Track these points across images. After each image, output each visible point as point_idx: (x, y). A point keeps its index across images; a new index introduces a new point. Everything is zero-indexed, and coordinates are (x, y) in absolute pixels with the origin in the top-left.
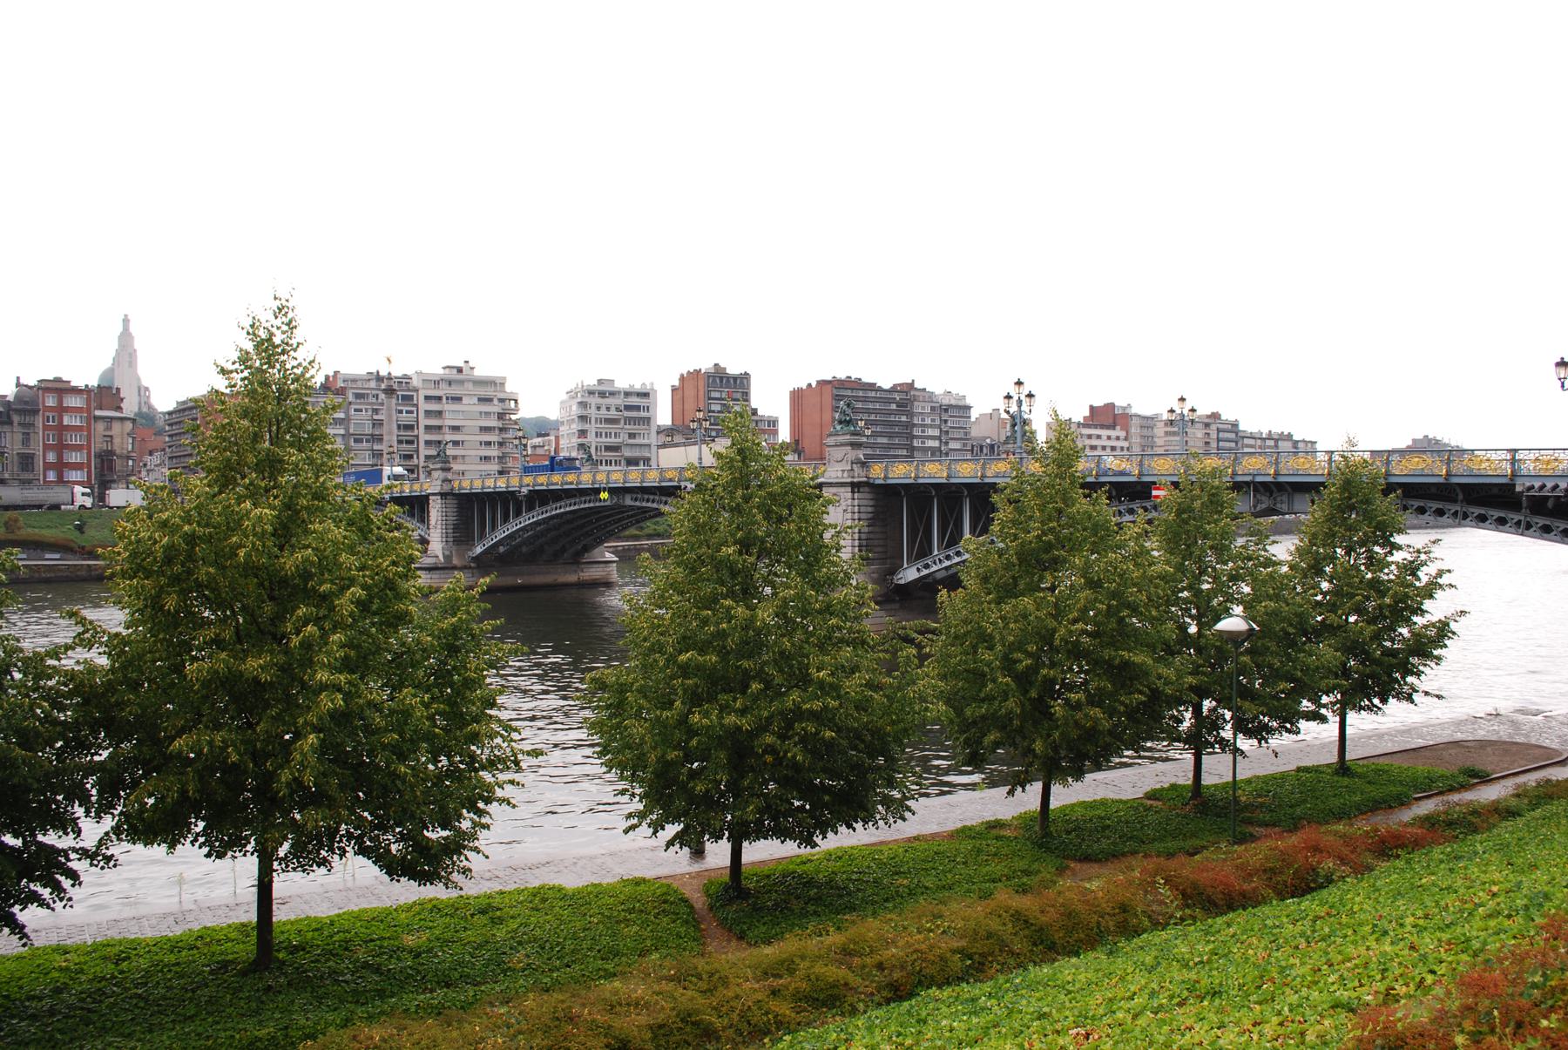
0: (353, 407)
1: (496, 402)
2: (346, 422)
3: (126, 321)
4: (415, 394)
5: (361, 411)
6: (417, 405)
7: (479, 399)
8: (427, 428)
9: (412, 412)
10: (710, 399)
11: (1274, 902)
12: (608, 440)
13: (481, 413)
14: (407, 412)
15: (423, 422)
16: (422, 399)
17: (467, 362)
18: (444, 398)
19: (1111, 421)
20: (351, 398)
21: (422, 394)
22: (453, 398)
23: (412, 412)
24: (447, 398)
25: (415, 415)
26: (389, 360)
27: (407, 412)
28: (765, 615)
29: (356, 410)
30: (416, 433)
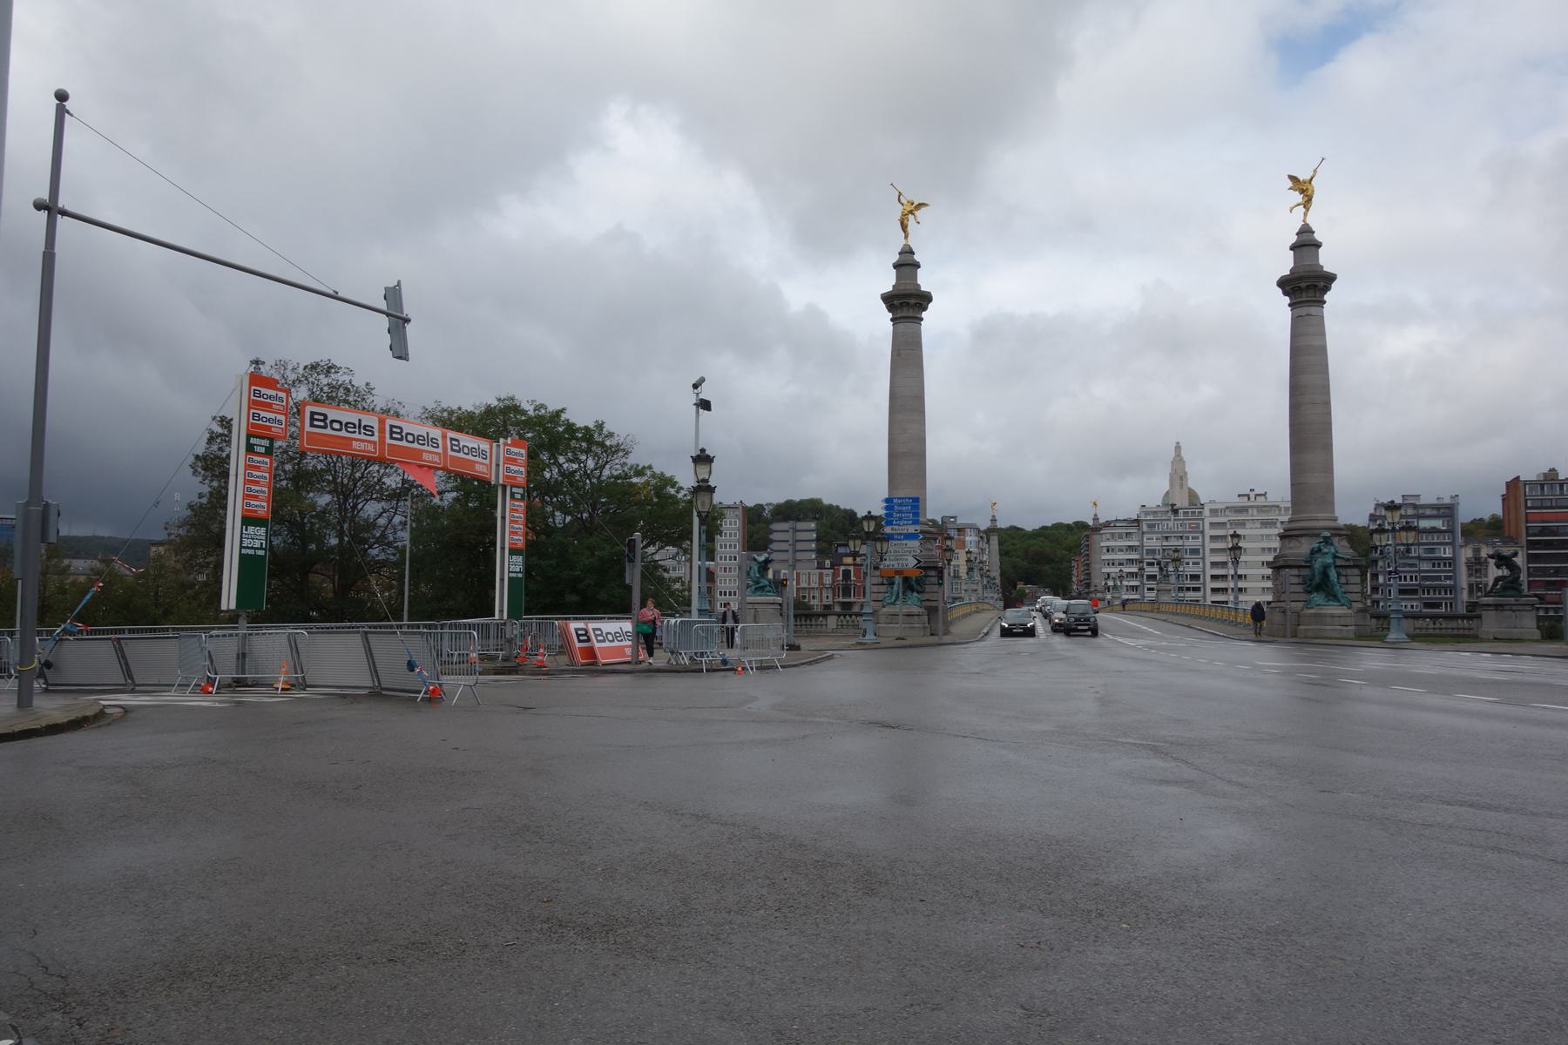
0: (1145, 536)
3: (1178, 447)
4: (1201, 522)
6: (1202, 532)
8: (1212, 550)
9: (1198, 538)
13: (1262, 535)
15: (1210, 572)
20: (1145, 528)
24: (1231, 524)
25: (1200, 540)
30: (1201, 555)
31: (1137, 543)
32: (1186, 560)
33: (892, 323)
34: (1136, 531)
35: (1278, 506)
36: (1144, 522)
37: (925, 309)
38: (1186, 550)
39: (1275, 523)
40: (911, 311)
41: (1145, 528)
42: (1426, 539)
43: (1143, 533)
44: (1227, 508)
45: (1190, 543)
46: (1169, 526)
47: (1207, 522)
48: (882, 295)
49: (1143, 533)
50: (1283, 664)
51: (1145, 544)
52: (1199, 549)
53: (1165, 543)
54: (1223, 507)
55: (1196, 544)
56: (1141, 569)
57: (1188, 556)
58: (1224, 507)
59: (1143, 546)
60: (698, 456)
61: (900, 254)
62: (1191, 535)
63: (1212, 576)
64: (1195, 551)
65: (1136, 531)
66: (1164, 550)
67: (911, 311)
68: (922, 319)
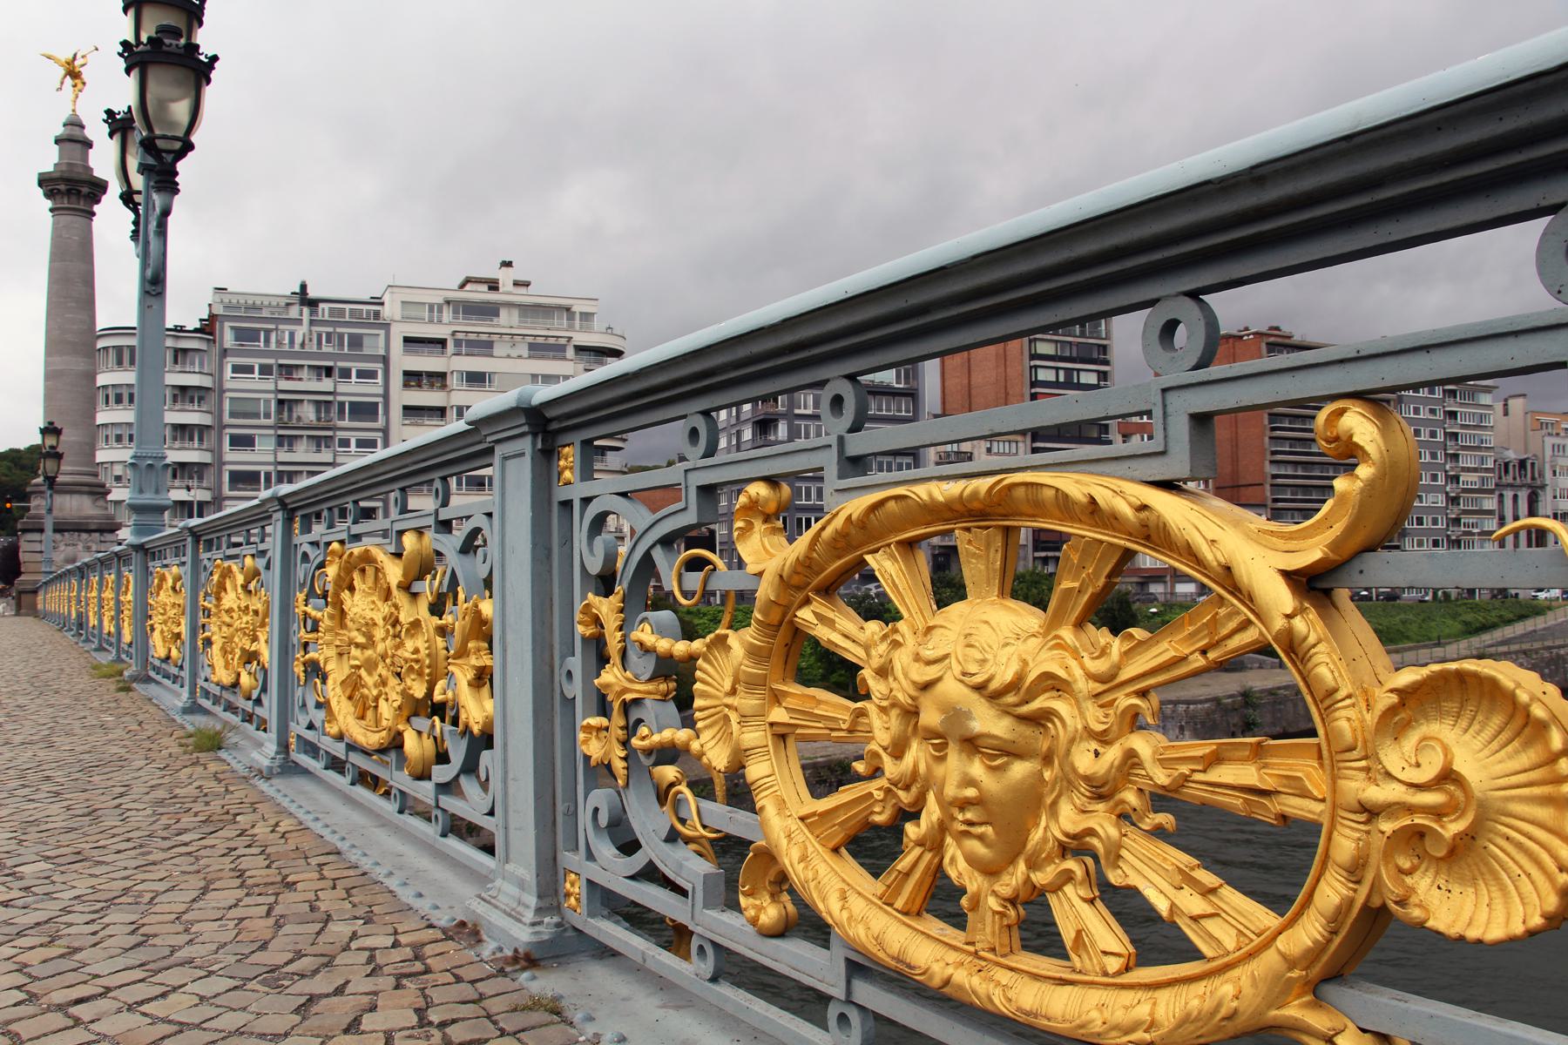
0: (230, 361)
1: (570, 353)
2: (213, 397)
4: (382, 332)
5: (250, 369)
6: (385, 360)
7: (532, 347)
8: (409, 410)
9: (371, 374)
10: (1034, 357)
11: (1057, 861)
12: (771, 751)
14: (362, 374)
15: (403, 396)
16: (397, 344)
17: (508, 264)
18: (450, 344)
19: (23, 596)
20: (229, 340)
21: (398, 332)
22: (470, 343)
23: (371, 374)
24: (458, 343)
25: (380, 380)
26: (73, 74)
27: (362, 374)
28: (734, 640)
29: (236, 369)
30: (380, 423)
31: (206, 382)
32: (341, 434)
33: (51, 214)
34: (203, 346)
35: (568, 309)
36: (227, 325)
37: (98, 202)
38: (342, 404)
39: (562, 348)
40: (82, 202)
41: (229, 340)
42: (888, 410)
43: (225, 353)
44: (448, 302)
45: (353, 390)
46: (298, 339)
47: (398, 332)
48: (40, 174)
49: (225, 353)
50: (262, 409)
51: (228, 385)
52: (377, 404)
53: (284, 385)
54: (438, 298)
55: (368, 391)
56: (217, 452)
57: (346, 423)
58: (440, 300)
59: (222, 391)
60: (46, 428)
61: (64, 125)
62: (355, 366)
63: (406, 408)
64: (364, 410)
65: (203, 346)
66: (281, 402)
67: (82, 202)
68: (94, 214)
